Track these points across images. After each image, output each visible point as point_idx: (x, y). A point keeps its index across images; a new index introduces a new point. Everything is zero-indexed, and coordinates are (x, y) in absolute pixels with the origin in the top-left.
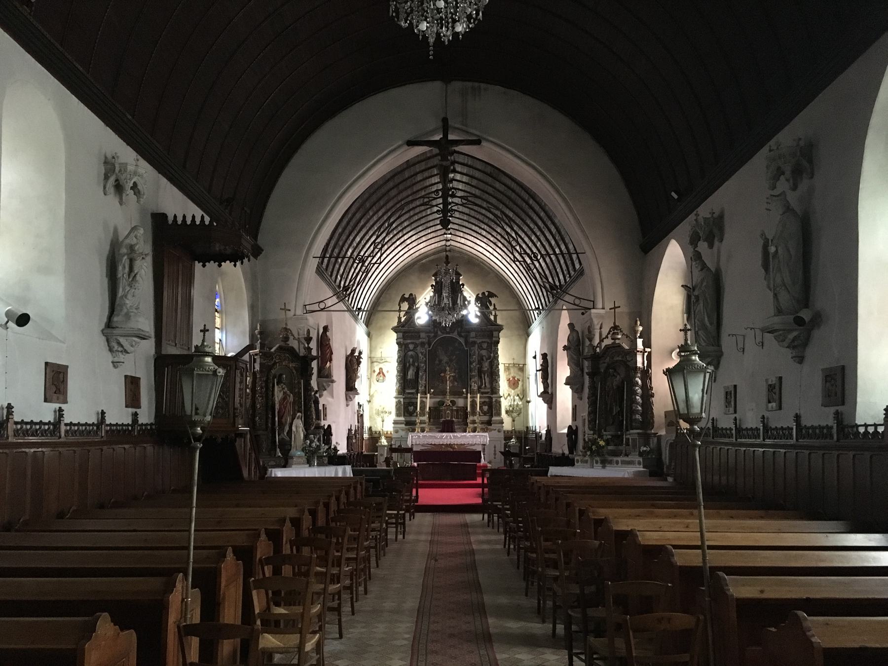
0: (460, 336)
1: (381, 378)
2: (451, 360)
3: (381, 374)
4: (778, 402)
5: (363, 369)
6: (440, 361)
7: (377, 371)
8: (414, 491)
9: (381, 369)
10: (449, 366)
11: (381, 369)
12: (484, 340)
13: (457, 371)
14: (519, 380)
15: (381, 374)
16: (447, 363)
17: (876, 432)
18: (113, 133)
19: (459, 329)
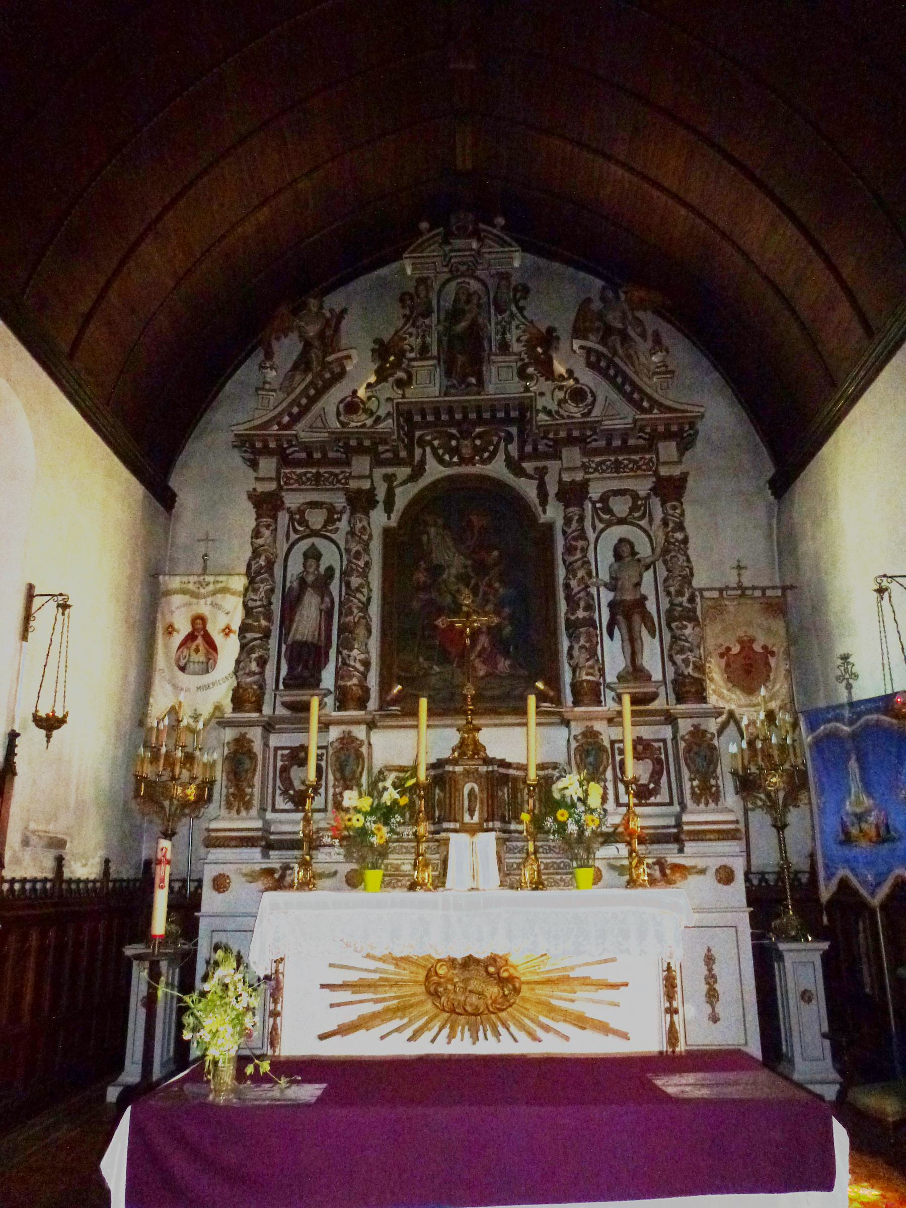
0: (518, 471)
1: (201, 657)
2: (481, 568)
3: (200, 641)
4: (744, 841)
5: (372, 952)
6: (436, 570)
7: (184, 628)
8: (384, 456)
9: (199, 621)
10: (475, 592)
11: (199, 621)
12: (615, 485)
13: (507, 610)
14: (768, 651)
15: (200, 641)
16: (464, 579)
17: (44, 889)
18: (569, 1204)
19: (513, 449)
